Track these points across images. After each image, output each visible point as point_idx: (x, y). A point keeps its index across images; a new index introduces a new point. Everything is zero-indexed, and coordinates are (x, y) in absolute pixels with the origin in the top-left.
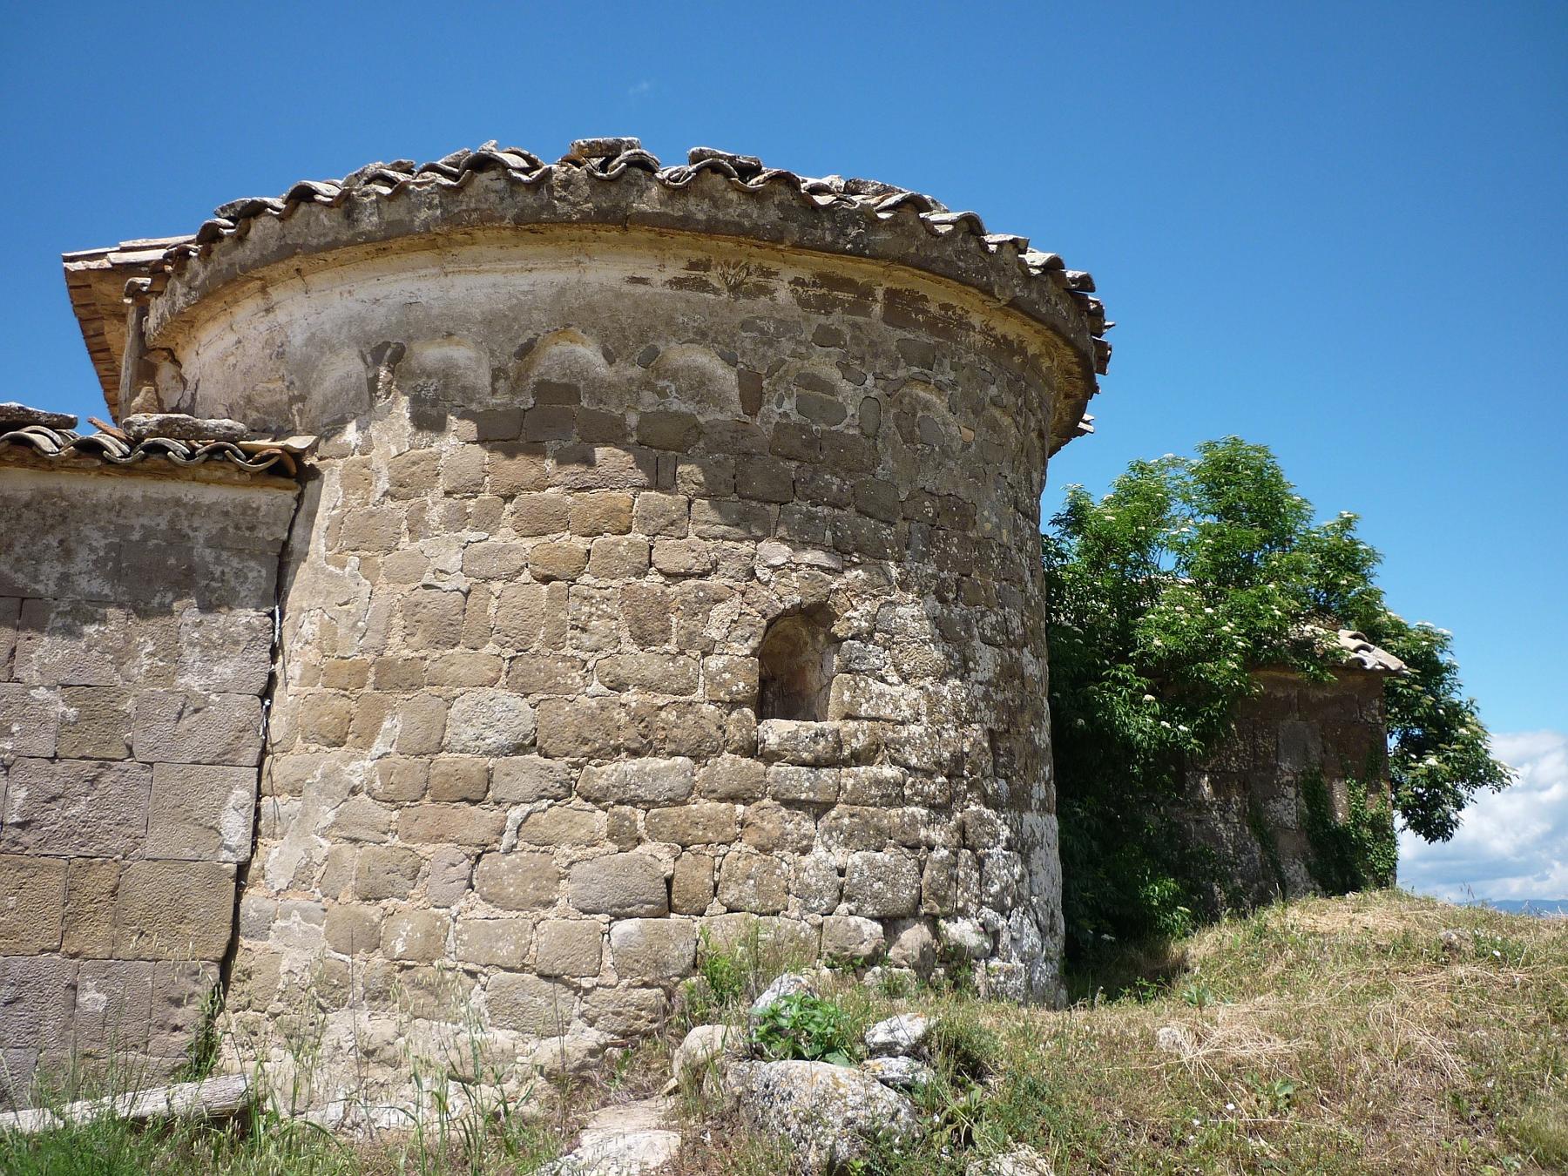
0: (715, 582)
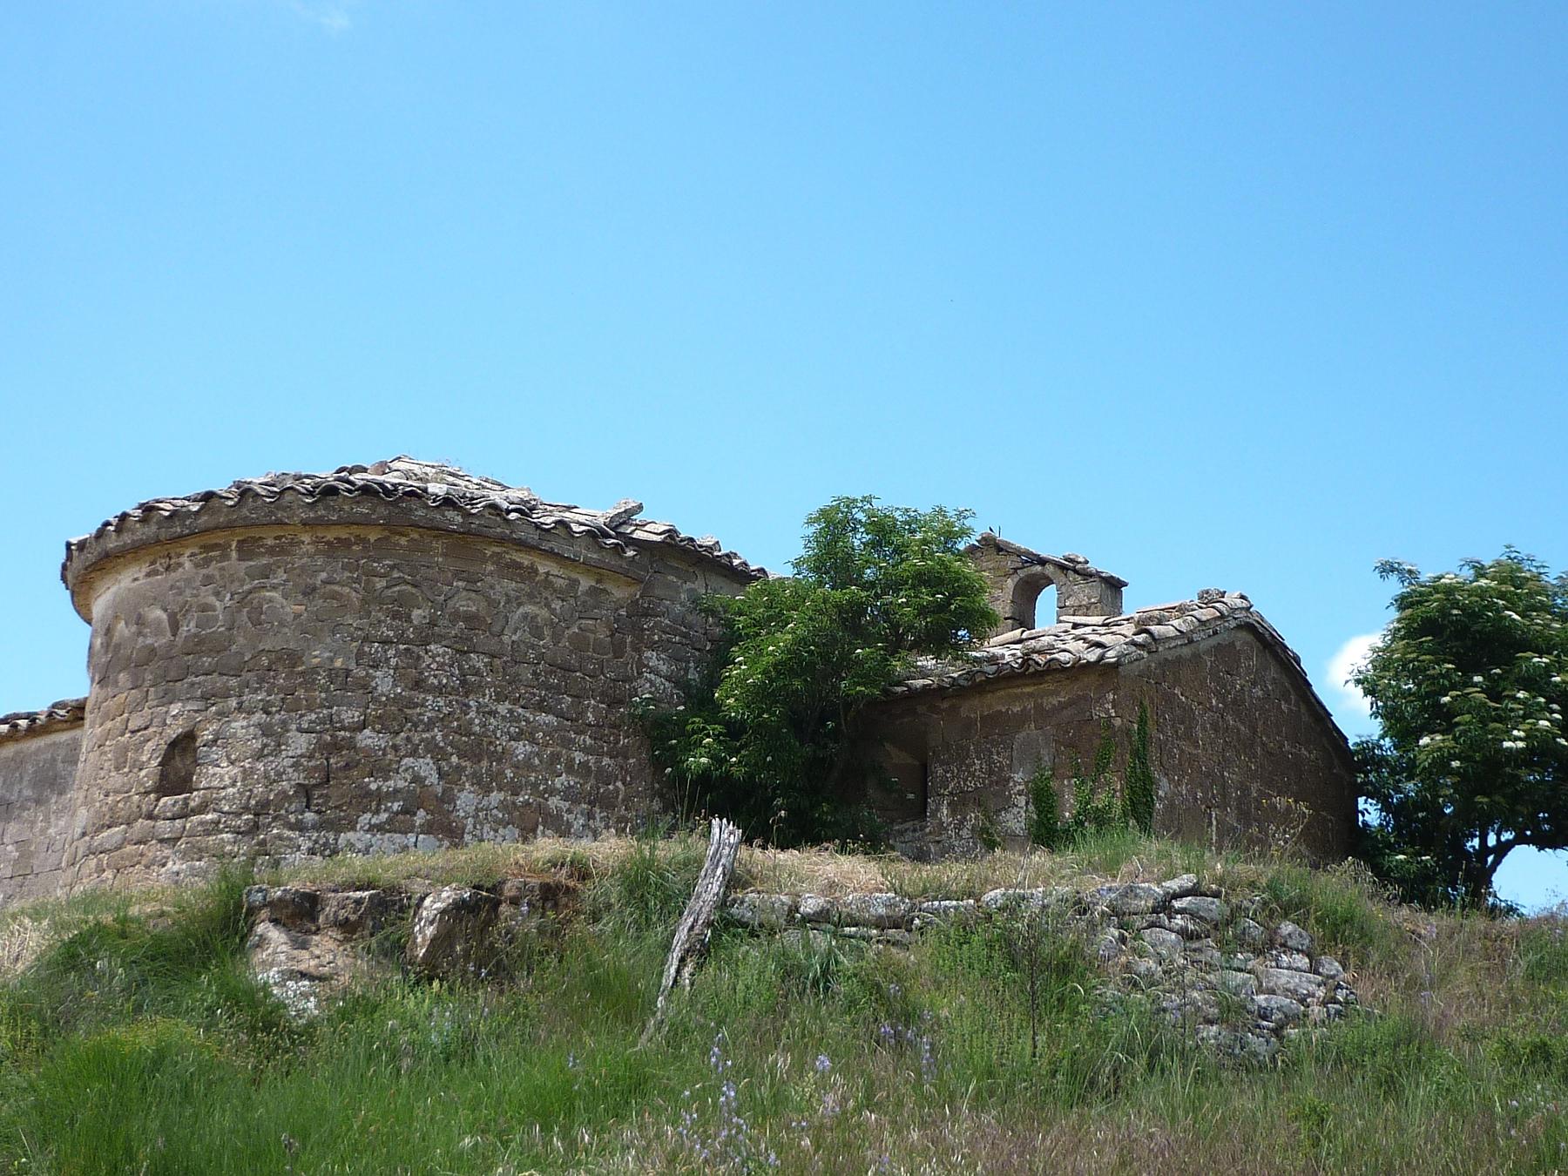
0: (151, 730)
